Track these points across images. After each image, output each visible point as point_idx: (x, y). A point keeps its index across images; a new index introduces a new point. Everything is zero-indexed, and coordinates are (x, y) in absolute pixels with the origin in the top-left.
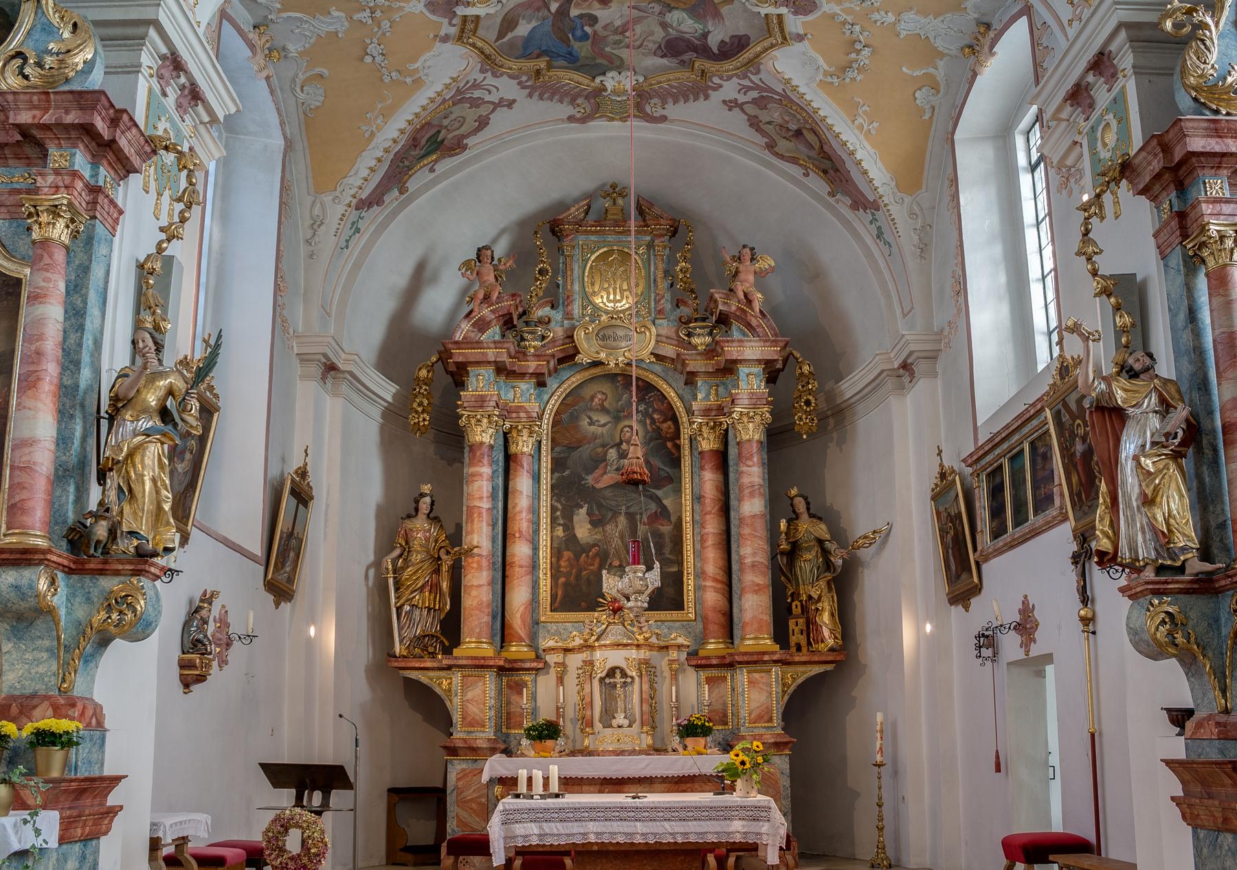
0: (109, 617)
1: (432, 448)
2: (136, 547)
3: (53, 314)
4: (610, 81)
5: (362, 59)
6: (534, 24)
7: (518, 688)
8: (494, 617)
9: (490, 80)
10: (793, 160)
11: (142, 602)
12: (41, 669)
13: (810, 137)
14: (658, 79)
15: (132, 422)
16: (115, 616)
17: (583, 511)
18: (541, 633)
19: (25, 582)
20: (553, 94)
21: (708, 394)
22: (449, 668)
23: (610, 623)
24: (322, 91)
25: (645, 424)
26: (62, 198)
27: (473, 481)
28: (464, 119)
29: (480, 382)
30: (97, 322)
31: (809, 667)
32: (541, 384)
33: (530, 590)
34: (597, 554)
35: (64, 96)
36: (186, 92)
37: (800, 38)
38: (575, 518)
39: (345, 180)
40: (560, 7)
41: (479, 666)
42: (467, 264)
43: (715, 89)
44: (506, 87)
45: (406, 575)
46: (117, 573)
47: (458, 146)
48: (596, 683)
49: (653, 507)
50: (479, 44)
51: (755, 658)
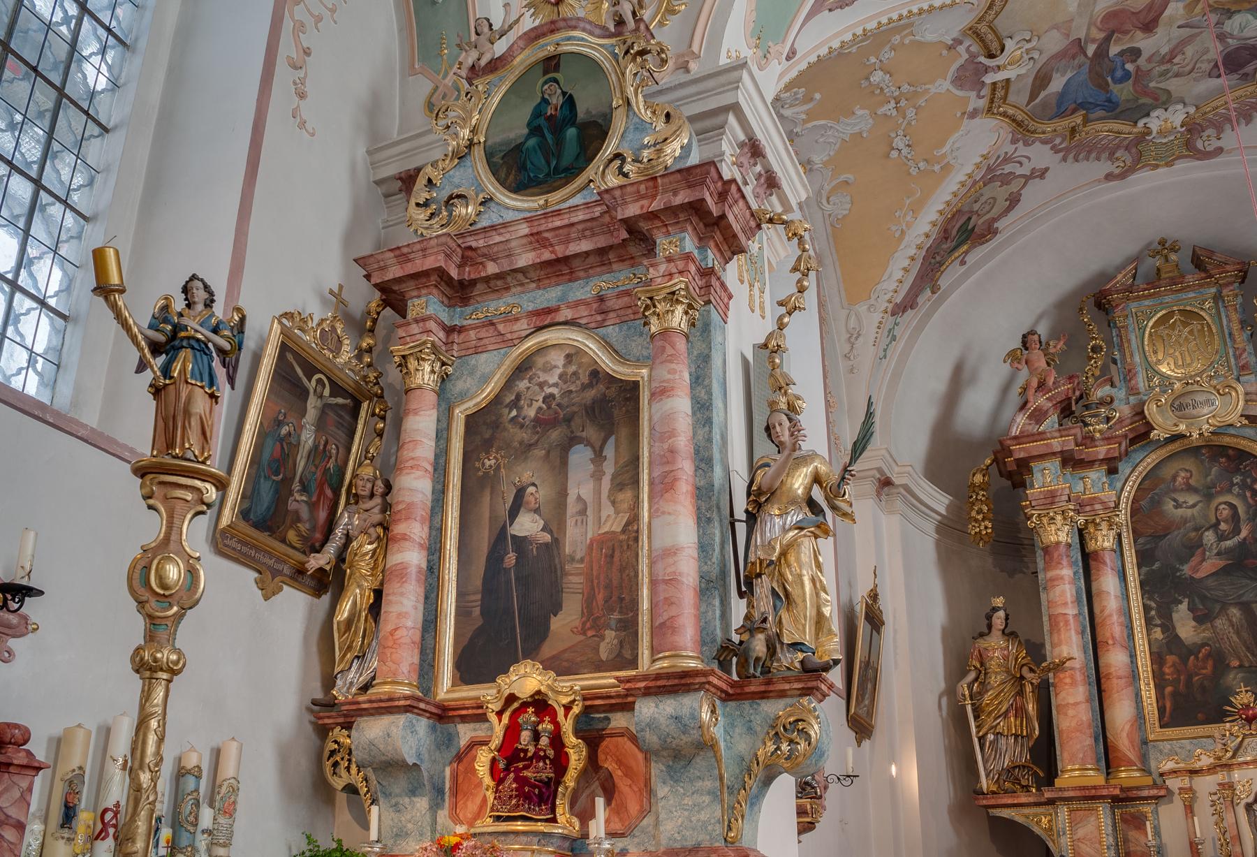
0: (778, 748)
1: (990, 560)
2: (802, 662)
3: (681, 405)
4: (1155, 122)
5: (887, 156)
6: (1069, 75)
7: (1138, 822)
8: (1096, 740)
9: (1022, 150)
11: (816, 727)
12: (703, 816)
14: (1214, 104)
15: (780, 516)
16: (785, 747)
17: (1184, 607)
18: (1153, 755)
19: (685, 711)
20: (1089, 152)
22: (1051, 802)
23: (1245, 736)
24: (848, 198)
25: (1242, 497)
26: (679, 282)
27: (1054, 586)
28: (994, 199)
29: (1046, 477)
30: (722, 414)
32: (1112, 471)
33: (1134, 704)
34: (1209, 655)
35: (672, 178)
36: (762, 180)
38: (1175, 616)
39: (879, 287)
40: (1098, 48)
41: (1089, 797)
42: (1013, 356)
44: (1039, 155)
45: (987, 698)
46: (782, 694)
47: (990, 231)
48: (1241, 811)
50: (1011, 111)
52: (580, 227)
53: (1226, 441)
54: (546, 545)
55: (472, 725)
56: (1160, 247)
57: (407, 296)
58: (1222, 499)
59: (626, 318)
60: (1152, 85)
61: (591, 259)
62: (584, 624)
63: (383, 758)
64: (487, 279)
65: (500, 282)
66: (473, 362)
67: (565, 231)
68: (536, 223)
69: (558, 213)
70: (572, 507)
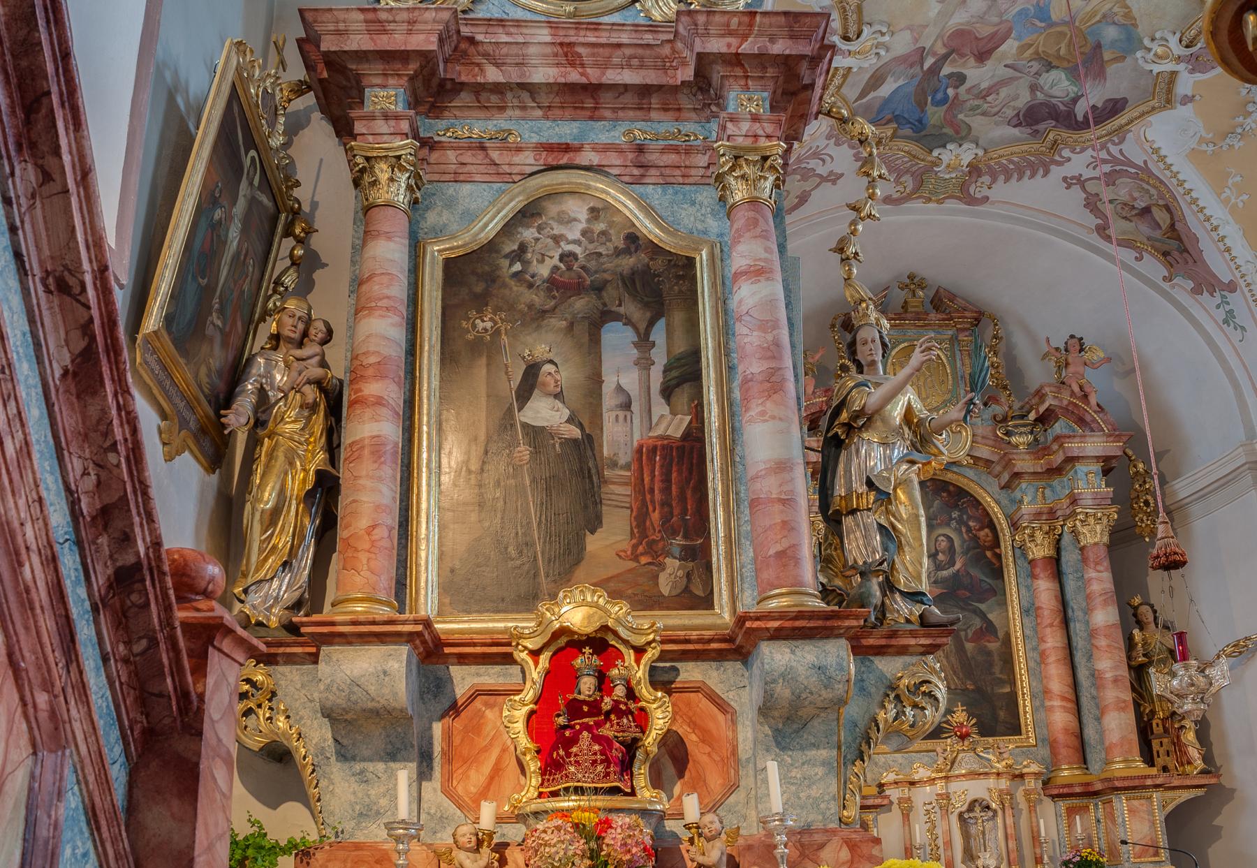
6: (900, 82)
10: (1125, 243)
12: (815, 792)
13: (1161, 216)
14: (1001, 152)
21: (1035, 498)
31: (1178, 792)
35: (774, 19)
37: (1187, 100)
40: (935, 63)
43: (1059, 164)
46: (903, 651)
48: (954, 819)
49: (977, 623)
51: (1136, 783)
52: (628, 52)
53: (949, 477)
54: (575, 441)
55: (473, 668)
56: (908, 281)
57: (365, 82)
58: (941, 531)
59: (672, 180)
60: (961, 116)
61: (629, 99)
62: (635, 547)
63: (370, 705)
64: (479, 89)
65: (493, 96)
66: (451, 191)
67: (607, 51)
68: (561, 33)
69: (596, 27)
70: (609, 400)
